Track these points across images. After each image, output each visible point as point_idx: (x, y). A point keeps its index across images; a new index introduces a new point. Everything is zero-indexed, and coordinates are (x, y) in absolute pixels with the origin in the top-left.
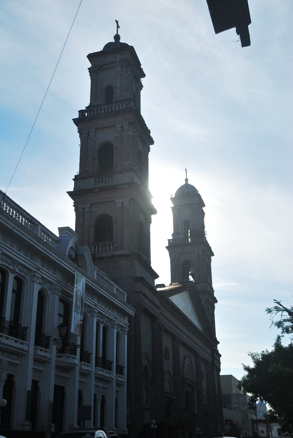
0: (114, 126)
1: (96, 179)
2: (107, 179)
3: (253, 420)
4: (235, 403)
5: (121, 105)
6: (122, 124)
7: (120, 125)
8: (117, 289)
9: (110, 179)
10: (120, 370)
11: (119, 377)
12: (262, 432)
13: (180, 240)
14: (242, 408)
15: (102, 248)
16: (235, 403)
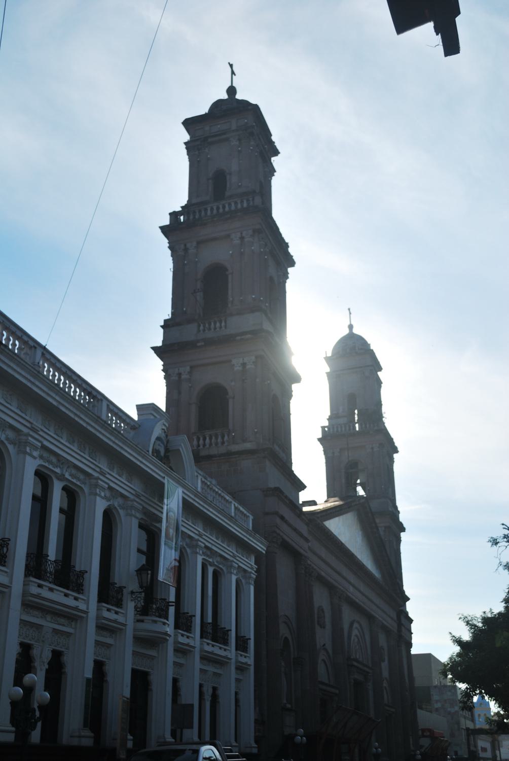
0: (228, 236)
3: (468, 729)
4: (437, 701)
5: (239, 202)
7: (239, 235)
9: (223, 324)
11: (241, 655)
12: (484, 750)
13: (341, 427)
14: (449, 709)
16: (437, 701)
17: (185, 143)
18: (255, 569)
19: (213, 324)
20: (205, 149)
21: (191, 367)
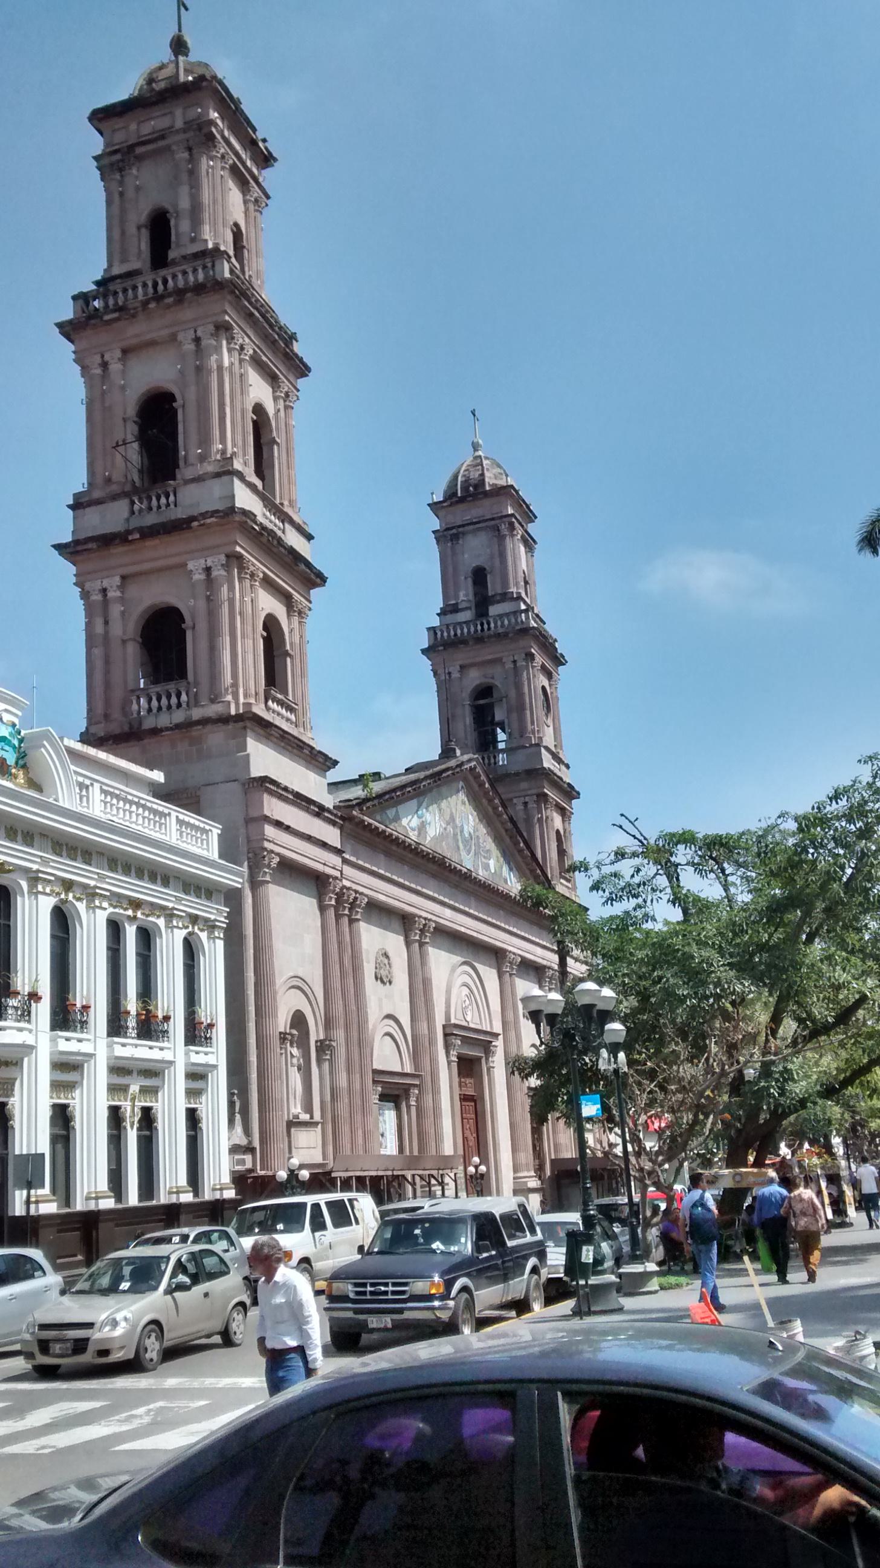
0: (173, 338)
1: (133, 503)
2: (163, 500)
5: (190, 271)
6: (195, 331)
7: (191, 334)
8: (180, 822)
9: (172, 498)
10: (196, 1034)
11: (197, 1053)
15: (159, 700)
17: (97, 158)
18: (226, 915)
19: (154, 498)
20: (130, 169)
21: (124, 578)
